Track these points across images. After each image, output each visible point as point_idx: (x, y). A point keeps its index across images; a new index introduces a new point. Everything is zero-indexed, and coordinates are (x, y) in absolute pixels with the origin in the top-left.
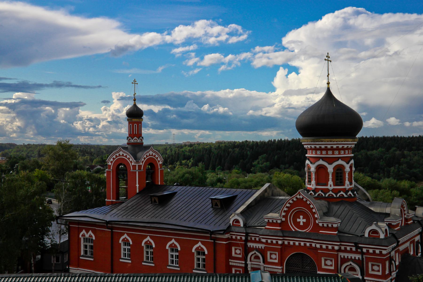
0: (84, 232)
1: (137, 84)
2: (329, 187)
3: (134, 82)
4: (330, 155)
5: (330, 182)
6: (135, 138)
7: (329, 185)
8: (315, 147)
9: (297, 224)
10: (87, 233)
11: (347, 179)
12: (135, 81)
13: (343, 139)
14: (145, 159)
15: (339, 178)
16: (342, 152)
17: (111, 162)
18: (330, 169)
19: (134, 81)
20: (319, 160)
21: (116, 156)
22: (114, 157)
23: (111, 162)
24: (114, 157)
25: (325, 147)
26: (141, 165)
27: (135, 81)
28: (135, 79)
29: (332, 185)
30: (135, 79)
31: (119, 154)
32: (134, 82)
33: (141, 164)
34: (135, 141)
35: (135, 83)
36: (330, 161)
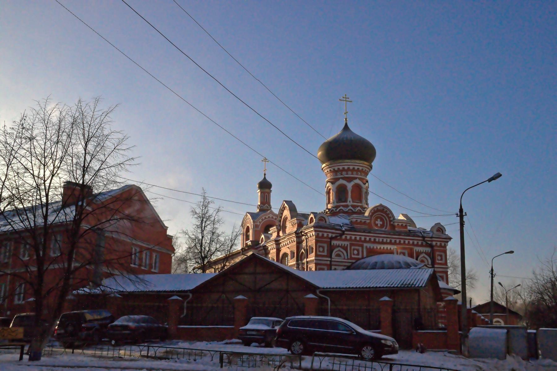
2: (348, 203)
4: (350, 175)
5: (350, 199)
7: (348, 202)
9: (377, 225)
16: (350, 173)
17: (260, 222)
18: (349, 186)
23: (260, 222)
26: (257, 225)
33: (258, 223)
36: (349, 180)
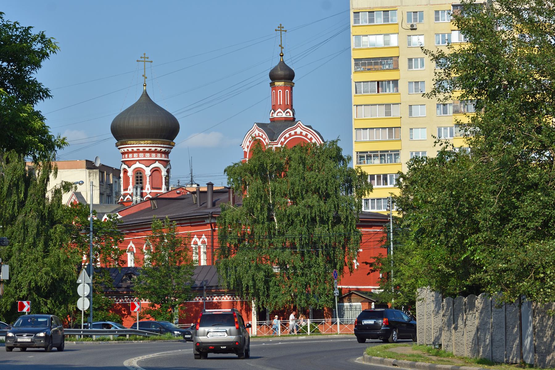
0: (195, 239)
1: (286, 31)
3: (280, 29)
6: (279, 110)
8: (133, 150)
10: (200, 238)
11: (148, 183)
12: (281, 27)
13: (134, 142)
14: (286, 139)
15: (139, 182)
18: (148, 171)
19: (279, 27)
20: (155, 163)
21: (290, 134)
22: (287, 135)
24: (287, 135)
25: (143, 149)
27: (281, 27)
28: (281, 25)
29: (150, 189)
30: (281, 25)
31: (296, 132)
32: (280, 29)
34: (279, 114)
35: (281, 30)
